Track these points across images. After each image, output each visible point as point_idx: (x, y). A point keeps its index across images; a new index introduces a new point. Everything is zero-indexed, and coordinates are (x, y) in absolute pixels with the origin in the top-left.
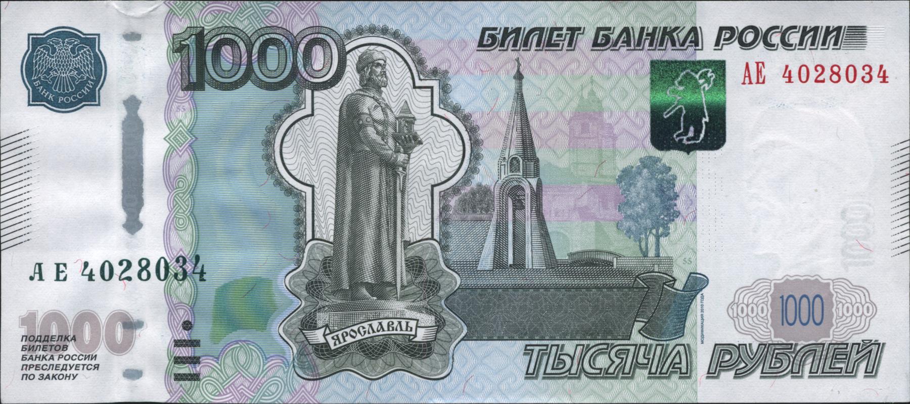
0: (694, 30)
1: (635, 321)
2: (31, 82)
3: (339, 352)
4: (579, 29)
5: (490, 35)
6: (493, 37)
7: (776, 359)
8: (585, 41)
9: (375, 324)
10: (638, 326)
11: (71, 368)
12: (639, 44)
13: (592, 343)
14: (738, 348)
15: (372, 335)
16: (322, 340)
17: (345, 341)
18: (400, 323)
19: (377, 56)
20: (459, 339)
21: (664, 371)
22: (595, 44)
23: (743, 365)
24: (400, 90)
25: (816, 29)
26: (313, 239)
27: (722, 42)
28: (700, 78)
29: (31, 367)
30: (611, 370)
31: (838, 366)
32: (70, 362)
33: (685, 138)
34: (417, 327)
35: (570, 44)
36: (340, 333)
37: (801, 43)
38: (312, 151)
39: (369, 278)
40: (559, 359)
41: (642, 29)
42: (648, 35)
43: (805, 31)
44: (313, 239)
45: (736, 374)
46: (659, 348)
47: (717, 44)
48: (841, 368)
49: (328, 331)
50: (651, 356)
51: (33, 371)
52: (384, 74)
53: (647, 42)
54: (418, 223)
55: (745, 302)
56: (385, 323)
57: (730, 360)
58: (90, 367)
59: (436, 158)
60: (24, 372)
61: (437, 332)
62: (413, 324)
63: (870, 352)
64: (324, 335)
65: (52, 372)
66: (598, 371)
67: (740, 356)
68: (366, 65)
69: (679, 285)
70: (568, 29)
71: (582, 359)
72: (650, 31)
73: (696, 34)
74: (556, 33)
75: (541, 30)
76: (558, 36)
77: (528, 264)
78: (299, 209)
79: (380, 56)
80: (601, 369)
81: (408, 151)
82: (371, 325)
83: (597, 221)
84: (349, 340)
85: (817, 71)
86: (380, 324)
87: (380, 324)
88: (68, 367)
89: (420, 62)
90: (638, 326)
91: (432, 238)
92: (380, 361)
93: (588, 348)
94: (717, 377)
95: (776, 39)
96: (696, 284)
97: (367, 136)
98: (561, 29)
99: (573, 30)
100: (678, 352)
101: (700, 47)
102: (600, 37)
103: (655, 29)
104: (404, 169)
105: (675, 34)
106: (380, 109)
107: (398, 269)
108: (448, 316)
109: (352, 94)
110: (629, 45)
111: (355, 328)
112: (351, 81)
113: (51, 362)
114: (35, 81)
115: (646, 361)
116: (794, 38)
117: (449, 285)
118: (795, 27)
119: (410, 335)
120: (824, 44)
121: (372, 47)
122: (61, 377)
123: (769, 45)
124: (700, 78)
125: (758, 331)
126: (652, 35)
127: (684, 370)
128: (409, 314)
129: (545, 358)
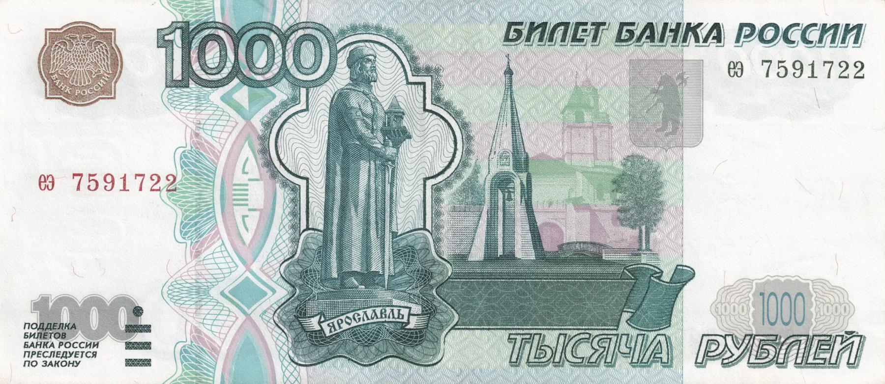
0: (716, 26)
1: (623, 311)
2: (49, 76)
3: (333, 338)
6: (631, 33)
7: (765, 349)
8: (608, 35)
9: (369, 312)
10: (626, 316)
11: (71, 355)
12: (662, 40)
14: (725, 337)
15: (366, 322)
16: (317, 328)
17: (340, 328)
18: (392, 310)
19: (366, 51)
20: (449, 328)
22: (619, 39)
23: (729, 354)
24: (390, 84)
25: (836, 26)
26: (308, 229)
27: (742, 39)
29: (34, 353)
30: (593, 360)
31: (822, 356)
32: (71, 350)
34: (410, 315)
36: (335, 320)
37: (820, 41)
38: (306, 143)
39: (356, 267)
41: (666, 24)
42: (671, 30)
43: (824, 29)
44: (308, 229)
46: (640, 338)
47: (738, 41)
48: (825, 359)
49: (323, 319)
50: (633, 345)
51: (35, 358)
52: (374, 69)
53: (671, 39)
54: (406, 216)
56: (378, 310)
57: (710, 351)
58: (89, 354)
59: (425, 151)
60: (27, 359)
61: (429, 320)
62: (405, 312)
63: (853, 343)
64: (320, 323)
65: (54, 360)
66: (580, 361)
67: (726, 345)
68: (356, 61)
69: (666, 277)
70: (593, 24)
72: (674, 27)
73: (719, 33)
74: (581, 28)
75: (566, 25)
76: (585, 31)
77: (519, 255)
78: (295, 201)
79: (371, 52)
81: (397, 145)
82: (365, 313)
83: (593, 213)
84: (345, 326)
85: (841, 67)
86: (374, 311)
87: (374, 311)
88: (68, 355)
89: (413, 59)
90: (626, 316)
91: (424, 229)
92: (373, 349)
94: (705, 366)
95: (795, 35)
97: (356, 129)
98: (586, 24)
99: (598, 25)
102: (624, 33)
103: (678, 25)
104: (393, 162)
105: (698, 30)
106: (369, 103)
107: (386, 257)
108: (438, 302)
109: (342, 89)
110: (653, 40)
111: (351, 315)
112: (342, 76)
113: (52, 349)
114: (52, 74)
115: (627, 351)
116: (814, 35)
117: (441, 273)
118: (815, 25)
119: (403, 323)
120: (843, 41)
121: (360, 44)
122: (64, 364)
123: (787, 41)
125: (747, 321)
126: (675, 31)
127: (665, 360)
128: (396, 302)
129: (528, 346)
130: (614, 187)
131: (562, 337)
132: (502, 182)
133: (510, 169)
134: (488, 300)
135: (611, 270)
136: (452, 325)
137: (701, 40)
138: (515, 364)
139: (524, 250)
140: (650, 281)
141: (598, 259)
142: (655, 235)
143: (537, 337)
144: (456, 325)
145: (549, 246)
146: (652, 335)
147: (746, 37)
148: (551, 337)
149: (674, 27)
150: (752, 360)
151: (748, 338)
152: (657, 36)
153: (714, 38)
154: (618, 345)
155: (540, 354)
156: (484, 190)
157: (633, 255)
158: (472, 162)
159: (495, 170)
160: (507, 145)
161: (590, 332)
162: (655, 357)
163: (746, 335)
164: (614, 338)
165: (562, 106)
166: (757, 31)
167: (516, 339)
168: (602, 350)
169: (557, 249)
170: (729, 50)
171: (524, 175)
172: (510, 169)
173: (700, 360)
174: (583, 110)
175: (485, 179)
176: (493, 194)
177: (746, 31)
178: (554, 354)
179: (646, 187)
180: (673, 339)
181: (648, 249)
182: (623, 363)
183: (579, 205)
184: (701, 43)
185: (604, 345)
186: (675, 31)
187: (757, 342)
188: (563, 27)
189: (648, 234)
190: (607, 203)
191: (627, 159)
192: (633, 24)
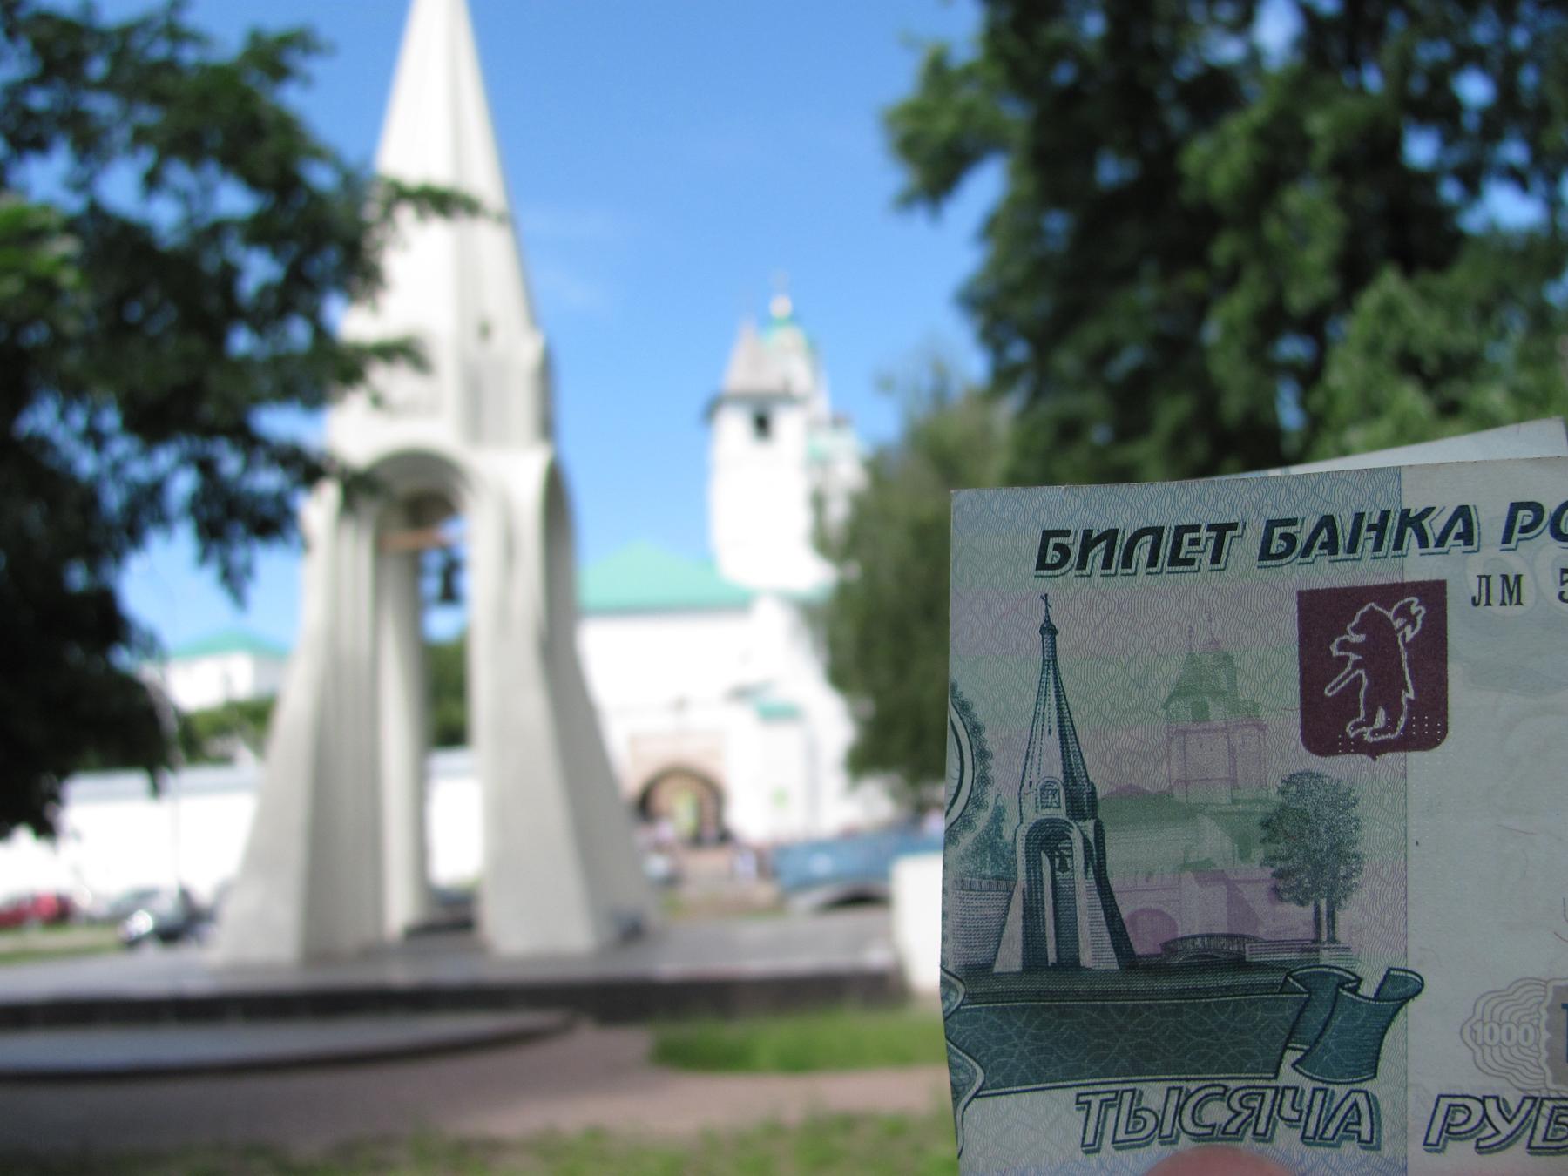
0: (1463, 513)
4: (1233, 526)
5: (1283, 536)
6: (1290, 539)
8: (1243, 549)
10: (1291, 1056)
13: (1193, 1086)
14: (1482, 1102)
21: (1329, 1134)
22: (1265, 554)
23: (1489, 1131)
27: (1516, 535)
28: (1396, 617)
30: (1232, 1128)
33: (1368, 730)
35: (1216, 559)
40: (1301, 1112)
41: (1359, 517)
42: (1371, 528)
45: (1477, 1147)
46: (1320, 1095)
47: (1507, 538)
53: (1370, 544)
55: (1496, 1018)
66: (1208, 1130)
67: (1485, 1115)
69: (1368, 989)
70: (1211, 528)
71: (1179, 1110)
72: (1375, 520)
73: (1468, 524)
74: (1187, 537)
75: (1157, 532)
76: (1195, 542)
77: (1086, 959)
80: (1213, 1126)
83: (1231, 886)
93: (1189, 1095)
96: (1401, 989)
98: (1196, 528)
99: (1220, 530)
100: (1355, 1104)
101: (1222, 565)
103: (1385, 515)
105: (1425, 522)
115: (1295, 1115)
124: (1396, 617)
126: (1380, 528)
127: (1366, 1136)
129: (1112, 1112)
130: (1264, 834)
131: (1174, 1094)
132: (1047, 839)
133: (1062, 814)
134: (1035, 1038)
135: (1261, 978)
136: (975, 1089)
137: (1432, 542)
138: (1091, 1149)
139: (1095, 951)
140: (1337, 996)
141: (1239, 964)
142: (1346, 918)
143: (1128, 1096)
144: (980, 1089)
145: (1144, 944)
146: (1340, 1091)
147: (1524, 530)
148: (1154, 1094)
149: (1375, 520)
150: (1538, 1142)
151: (1528, 1104)
152: (1343, 540)
153: (1458, 537)
154: (1277, 1105)
155: (1136, 1123)
156: (1014, 852)
157: (1303, 950)
158: (990, 800)
159: (1032, 817)
160: (1057, 773)
161: (1227, 1083)
162: (1349, 1130)
163: (1525, 1098)
164: (1270, 1094)
165: (1163, 693)
166: (1546, 518)
167: (1089, 1103)
168: (1247, 1112)
169: (1159, 950)
170: (1490, 556)
171: (1089, 825)
172: (1062, 814)
173: (1433, 1139)
174: (1207, 698)
175: (1015, 833)
176: (1033, 866)
177: (1525, 517)
178: (1159, 1124)
179: (1328, 830)
180: (1385, 1107)
181: (1332, 940)
182: (1286, 1139)
183: (1204, 872)
184: (1431, 548)
185: (1252, 1104)
186: (1380, 528)
187: (1545, 1111)
188: (1149, 538)
189: (1331, 916)
190: (1255, 871)
191: (1290, 780)
192: (1293, 522)
